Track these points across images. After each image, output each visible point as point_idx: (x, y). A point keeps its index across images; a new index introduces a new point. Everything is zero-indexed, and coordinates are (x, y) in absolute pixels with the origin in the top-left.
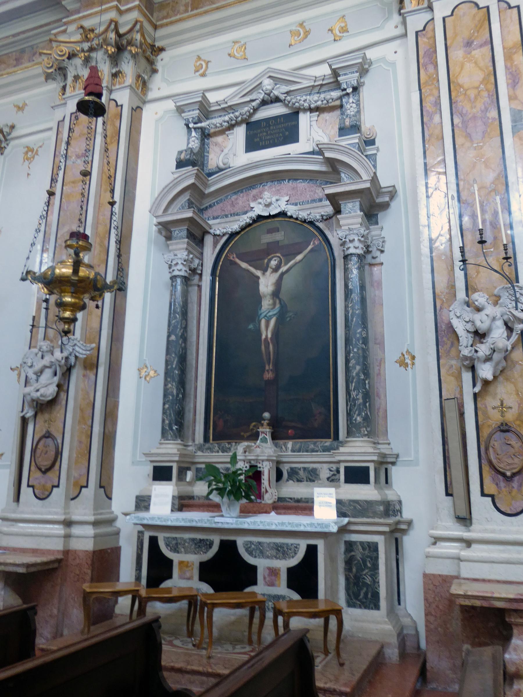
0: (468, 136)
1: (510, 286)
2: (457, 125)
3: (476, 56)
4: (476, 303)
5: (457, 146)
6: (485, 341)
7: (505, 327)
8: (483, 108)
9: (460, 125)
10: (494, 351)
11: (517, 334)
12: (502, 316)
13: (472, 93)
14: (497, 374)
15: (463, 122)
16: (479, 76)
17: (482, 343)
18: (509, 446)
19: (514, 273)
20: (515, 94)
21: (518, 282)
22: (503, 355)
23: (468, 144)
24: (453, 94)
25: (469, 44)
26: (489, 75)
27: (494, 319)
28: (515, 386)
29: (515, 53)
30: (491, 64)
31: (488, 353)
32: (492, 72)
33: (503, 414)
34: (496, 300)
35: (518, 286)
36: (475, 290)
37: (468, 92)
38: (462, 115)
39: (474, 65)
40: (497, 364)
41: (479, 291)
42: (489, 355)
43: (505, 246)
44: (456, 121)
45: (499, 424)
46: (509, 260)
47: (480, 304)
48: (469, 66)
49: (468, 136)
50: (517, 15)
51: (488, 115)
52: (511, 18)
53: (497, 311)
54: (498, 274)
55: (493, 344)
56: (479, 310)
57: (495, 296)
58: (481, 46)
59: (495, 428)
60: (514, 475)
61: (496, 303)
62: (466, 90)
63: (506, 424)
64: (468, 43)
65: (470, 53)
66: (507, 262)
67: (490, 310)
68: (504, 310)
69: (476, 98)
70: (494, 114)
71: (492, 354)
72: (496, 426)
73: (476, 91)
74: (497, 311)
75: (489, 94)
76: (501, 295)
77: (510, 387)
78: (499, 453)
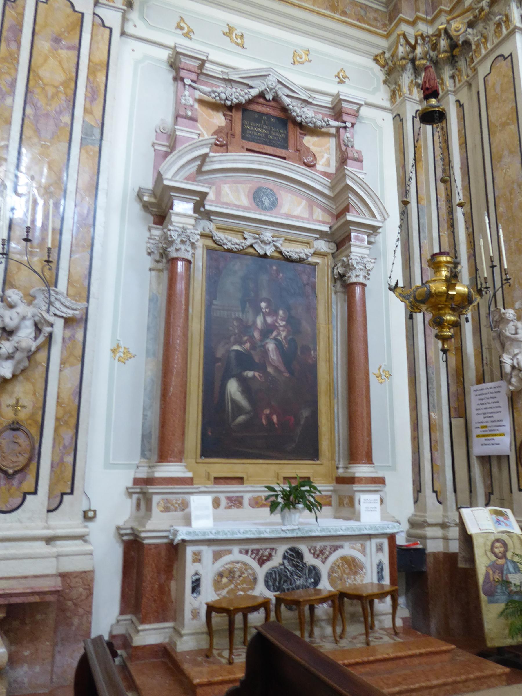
0: (37, 131)
1: (47, 288)
2: (28, 116)
3: (62, 56)
4: (9, 299)
5: (24, 137)
6: (11, 338)
7: (34, 328)
8: (58, 109)
9: (32, 117)
10: (17, 350)
11: (44, 336)
12: (33, 317)
13: (50, 91)
14: (17, 373)
15: (35, 115)
16: (59, 77)
17: (8, 340)
18: (17, 445)
19: (54, 277)
20: (91, 108)
21: (56, 286)
22: (25, 354)
23: (35, 140)
24: (31, 83)
25: (57, 40)
26: (70, 79)
27: (24, 318)
28: (34, 386)
29: (100, 70)
30: (74, 70)
31: (11, 351)
32: (74, 79)
33: (16, 412)
34: (30, 299)
35: (54, 291)
36: (12, 286)
37: (47, 88)
38: (35, 107)
39: (58, 63)
40: (19, 362)
41: (16, 288)
42: (12, 353)
43: (49, 249)
44: (29, 111)
45: (11, 421)
46: (50, 264)
47: (13, 301)
48: (52, 62)
49: (37, 131)
50: (108, 37)
51: (61, 118)
52: (102, 36)
53: (29, 311)
54: (38, 276)
55: (17, 343)
56: (11, 306)
57: (31, 296)
58: (69, 48)
59: (6, 426)
60: (16, 472)
61: (30, 303)
62: (45, 85)
63: (18, 423)
64: (56, 39)
65: (56, 50)
66: (48, 265)
67: (22, 309)
68: (35, 311)
69: (53, 97)
70: (66, 119)
71: (14, 353)
72: (7, 425)
73: (54, 90)
74: (29, 311)
75: (66, 99)
76: (37, 296)
77: (29, 387)
78: (5, 451)
